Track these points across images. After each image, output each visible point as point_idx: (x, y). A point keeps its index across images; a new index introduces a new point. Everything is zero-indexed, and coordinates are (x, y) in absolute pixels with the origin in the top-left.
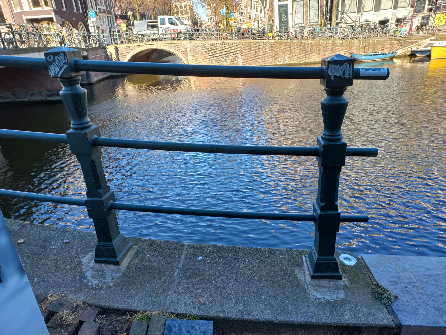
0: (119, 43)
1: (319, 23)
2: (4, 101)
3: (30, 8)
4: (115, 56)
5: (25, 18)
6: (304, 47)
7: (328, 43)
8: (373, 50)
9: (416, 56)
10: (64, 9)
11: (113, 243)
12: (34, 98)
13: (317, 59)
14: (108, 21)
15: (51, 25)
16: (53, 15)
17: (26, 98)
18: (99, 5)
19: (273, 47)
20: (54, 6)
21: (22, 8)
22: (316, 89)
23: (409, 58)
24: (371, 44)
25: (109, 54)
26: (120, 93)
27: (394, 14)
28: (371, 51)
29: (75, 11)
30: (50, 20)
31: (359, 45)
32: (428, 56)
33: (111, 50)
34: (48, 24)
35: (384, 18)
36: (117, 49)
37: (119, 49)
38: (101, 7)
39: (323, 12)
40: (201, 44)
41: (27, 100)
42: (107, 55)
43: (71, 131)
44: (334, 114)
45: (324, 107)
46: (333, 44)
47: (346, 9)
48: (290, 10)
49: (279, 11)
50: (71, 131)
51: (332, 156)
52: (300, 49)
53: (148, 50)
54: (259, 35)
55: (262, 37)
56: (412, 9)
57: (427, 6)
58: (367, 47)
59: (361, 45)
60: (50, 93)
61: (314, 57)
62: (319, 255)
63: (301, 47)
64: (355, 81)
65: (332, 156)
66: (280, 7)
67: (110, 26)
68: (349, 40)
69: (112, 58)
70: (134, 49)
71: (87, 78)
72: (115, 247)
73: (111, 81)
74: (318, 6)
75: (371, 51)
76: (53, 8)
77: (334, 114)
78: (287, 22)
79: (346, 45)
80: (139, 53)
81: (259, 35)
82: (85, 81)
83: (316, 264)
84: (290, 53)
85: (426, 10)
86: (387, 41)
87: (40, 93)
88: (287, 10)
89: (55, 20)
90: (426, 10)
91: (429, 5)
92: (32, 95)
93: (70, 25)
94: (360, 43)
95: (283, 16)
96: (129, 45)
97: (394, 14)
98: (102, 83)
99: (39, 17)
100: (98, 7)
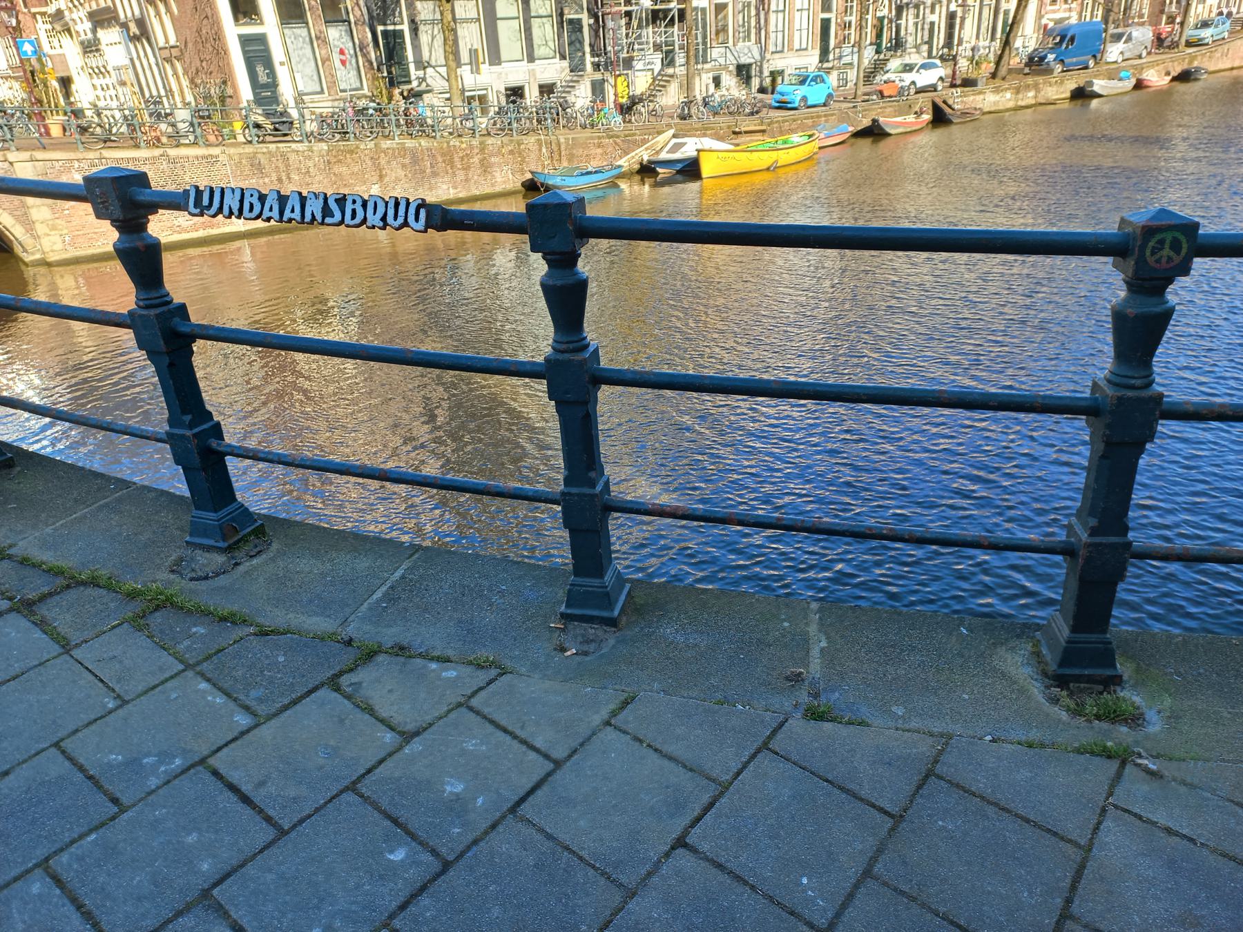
1: (366, 91)
6: (415, 160)
7: (471, 147)
8: (570, 161)
9: (658, 174)
13: (452, 191)
19: (329, 162)
22: (1106, 283)
23: (638, 178)
24: (563, 147)
27: (532, 73)
28: (565, 164)
31: (540, 150)
32: (690, 170)
35: (514, 81)
39: (371, 64)
40: (76, 164)
44: (1140, 333)
45: (1119, 318)
46: (482, 150)
47: (426, 56)
48: (277, 54)
49: (245, 52)
51: (1125, 420)
52: (404, 166)
54: (276, 130)
55: (285, 135)
56: (566, 64)
57: (589, 59)
58: (556, 156)
59: (544, 150)
61: (445, 187)
62: (1074, 630)
63: (407, 161)
64: (1198, 262)
65: (1125, 420)
66: (245, 41)
68: (515, 137)
74: (351, 44)
75: (565, 164)
77: (1140, 333)
78: (273, 85)
79: (511, 152)
81: (276, 130)
83: (1066, 650)
84: (381, 177)
85: (589, 67)
86: (592, 138)
88: (267, 50)
90: (589, 67)
91: (593, 56)
94: (540, 145)
95: (260, 69)
97: (532, 73)
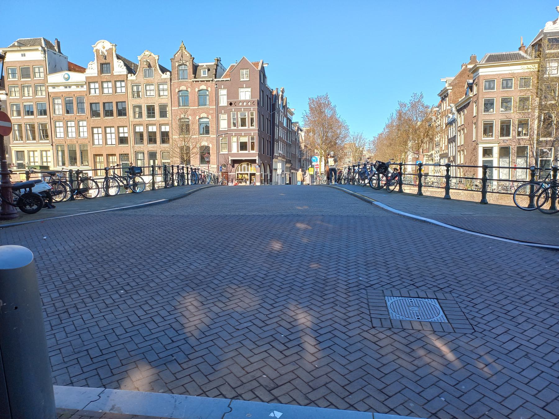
3: (238, 151)
5: (230, 158)
16: (257, 158)
30: (253, 161)
34: (248, 165)
89: (257, 162)
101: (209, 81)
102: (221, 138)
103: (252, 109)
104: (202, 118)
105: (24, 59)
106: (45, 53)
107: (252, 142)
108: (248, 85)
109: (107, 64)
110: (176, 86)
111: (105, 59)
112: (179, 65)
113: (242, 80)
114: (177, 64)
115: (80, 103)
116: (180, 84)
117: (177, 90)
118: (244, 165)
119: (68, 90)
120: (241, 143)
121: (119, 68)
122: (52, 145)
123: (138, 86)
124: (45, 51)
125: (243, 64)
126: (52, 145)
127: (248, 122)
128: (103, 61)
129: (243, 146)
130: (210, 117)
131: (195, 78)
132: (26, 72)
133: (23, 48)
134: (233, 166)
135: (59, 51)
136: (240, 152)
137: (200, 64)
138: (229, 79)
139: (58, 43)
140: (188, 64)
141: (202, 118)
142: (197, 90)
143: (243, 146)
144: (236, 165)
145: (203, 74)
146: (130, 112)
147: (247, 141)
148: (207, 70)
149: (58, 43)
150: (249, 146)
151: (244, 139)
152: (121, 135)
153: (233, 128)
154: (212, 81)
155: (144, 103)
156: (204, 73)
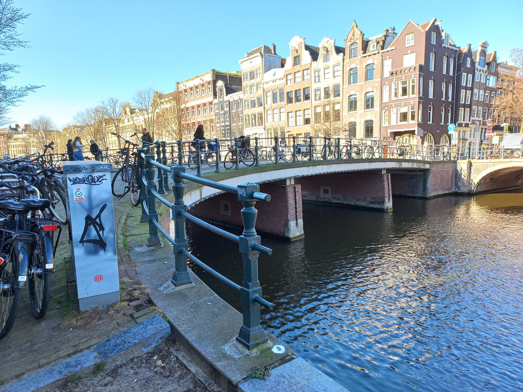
0: (477, 157)
2: (336, 201)
3: (397, 123)
4: (466, 172)
5: (389, 131)
10: (431, 122)
11: (251, 329)
12: (359, 203)
14: (481, 132)
15: (411, 137)
16: (416, 129)
17: (352, 202)
18: (474, 117)
20: (420, 120)
21: (389, 123)
25: (459, 169)
26: (461, 211)
29: (442, 123)
30: (412, 133)
33: (462, 165)
34: (410, 136)
36: (470, 165)
37: (473, 164)
38: (476, 118)
41: (353, 204)
42: (457, 170)
43: (242, 236)
50: (242, 236)
53: (513, 168)
60: (373, 200)
67: (483, 138)
69: (461, 173)
70: (494, 165)
71: (423, 191)
72: (251, 333)
73: (453, 199)
76: (418, 121)
80: (499, 170)
82: (420, 194)
87: (365, 200)
89: (416, 133)
92: (358, 200)
93: (432, 137)
96: (488, 160)
98: (440, 199)
99: (402, 130)
100: (472, 118)
101: (375, 54)
102: (384, 111)
103: (413, 76)
104: (368, 92)
105: (252, 65)
106: (262, 58)
107: (412, 112)
108: (412, 50)
109: (299, 56)
110: (347, 65)
111: (297, 52)
112: (351, 45)
113: (407, 46)
114: (349, 44)
115: (281, 94)
116: (350, 64)
117: (348, 69)
118: (406, 137)
119: (275, 84)
120: (242, 90)
121: (306, 56)
122: (265, 129)
123: (319, 71)
124: (262, 56)
125: (409, 29)
126: (265, 129)
127: (409, 90)
128: (296, 55)
129: (404, 117)
130: (375, 90)
131: (364, 53)
132: (252, 75)
133: (250, 57)
134: (394, 139)
135: (275, 53)
136: (400, 123)
137: (371, 39)
138: (394, 48)
139: (274, 47)
140: (358, 41)
141: (368, 92)
142: (364, 65)
143: (404, 117)
144: (397, 137)
145: (371, 47)
146: (312, 96)
147: (406, 111)
148: (375, 43)
149: (274, 47)
150: (409, 116)
151: (404, 110)
152: (306, 117)
153: (393, 98)
154: (378, 53)
155: (322, 85)
156: (373, 47)
